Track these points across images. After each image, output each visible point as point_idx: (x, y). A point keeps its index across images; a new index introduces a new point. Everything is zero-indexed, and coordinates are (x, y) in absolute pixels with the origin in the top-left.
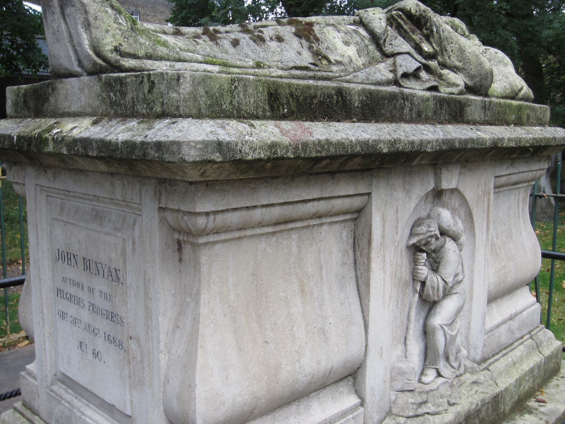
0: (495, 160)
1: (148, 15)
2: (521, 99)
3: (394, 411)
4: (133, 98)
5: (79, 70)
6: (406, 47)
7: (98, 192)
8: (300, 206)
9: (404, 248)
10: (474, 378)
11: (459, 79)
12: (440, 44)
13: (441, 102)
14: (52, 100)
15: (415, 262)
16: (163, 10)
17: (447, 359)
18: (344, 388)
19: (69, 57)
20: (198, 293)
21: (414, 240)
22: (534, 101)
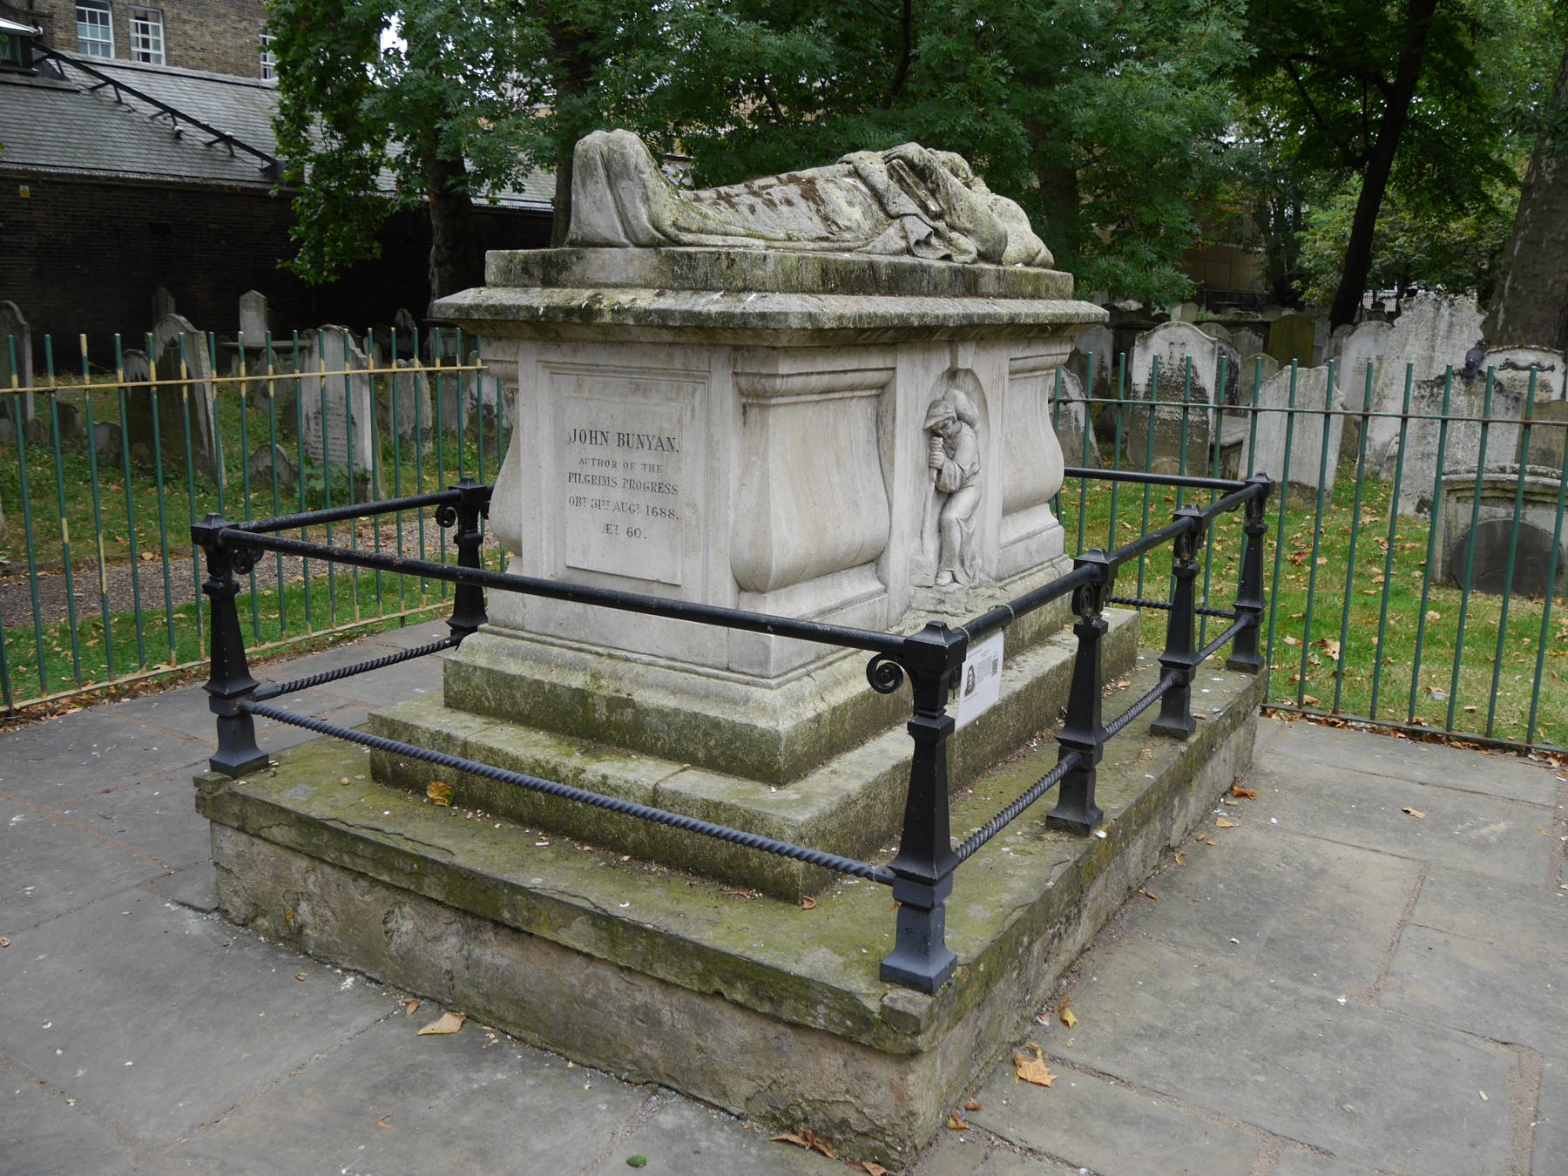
0: (499, 338)
1: (185, 22)
2: (1039, 265)
3: (914, 605)
5: (625, 241)
6: (912, 207)
7: (646, 363)
8: (842, 375)
9: (921, 432)
10: (991, 592)
11: (970, 244)
12: (947, 201)
13: (956, 272)
14: (577, 269)
15: (931, 447)
16: (223, 11)
17: (962, 563)
18: (868, 571)
19: (613, 228)
20: (766, 451)
21: (931, 423)
22: (1054, 268)
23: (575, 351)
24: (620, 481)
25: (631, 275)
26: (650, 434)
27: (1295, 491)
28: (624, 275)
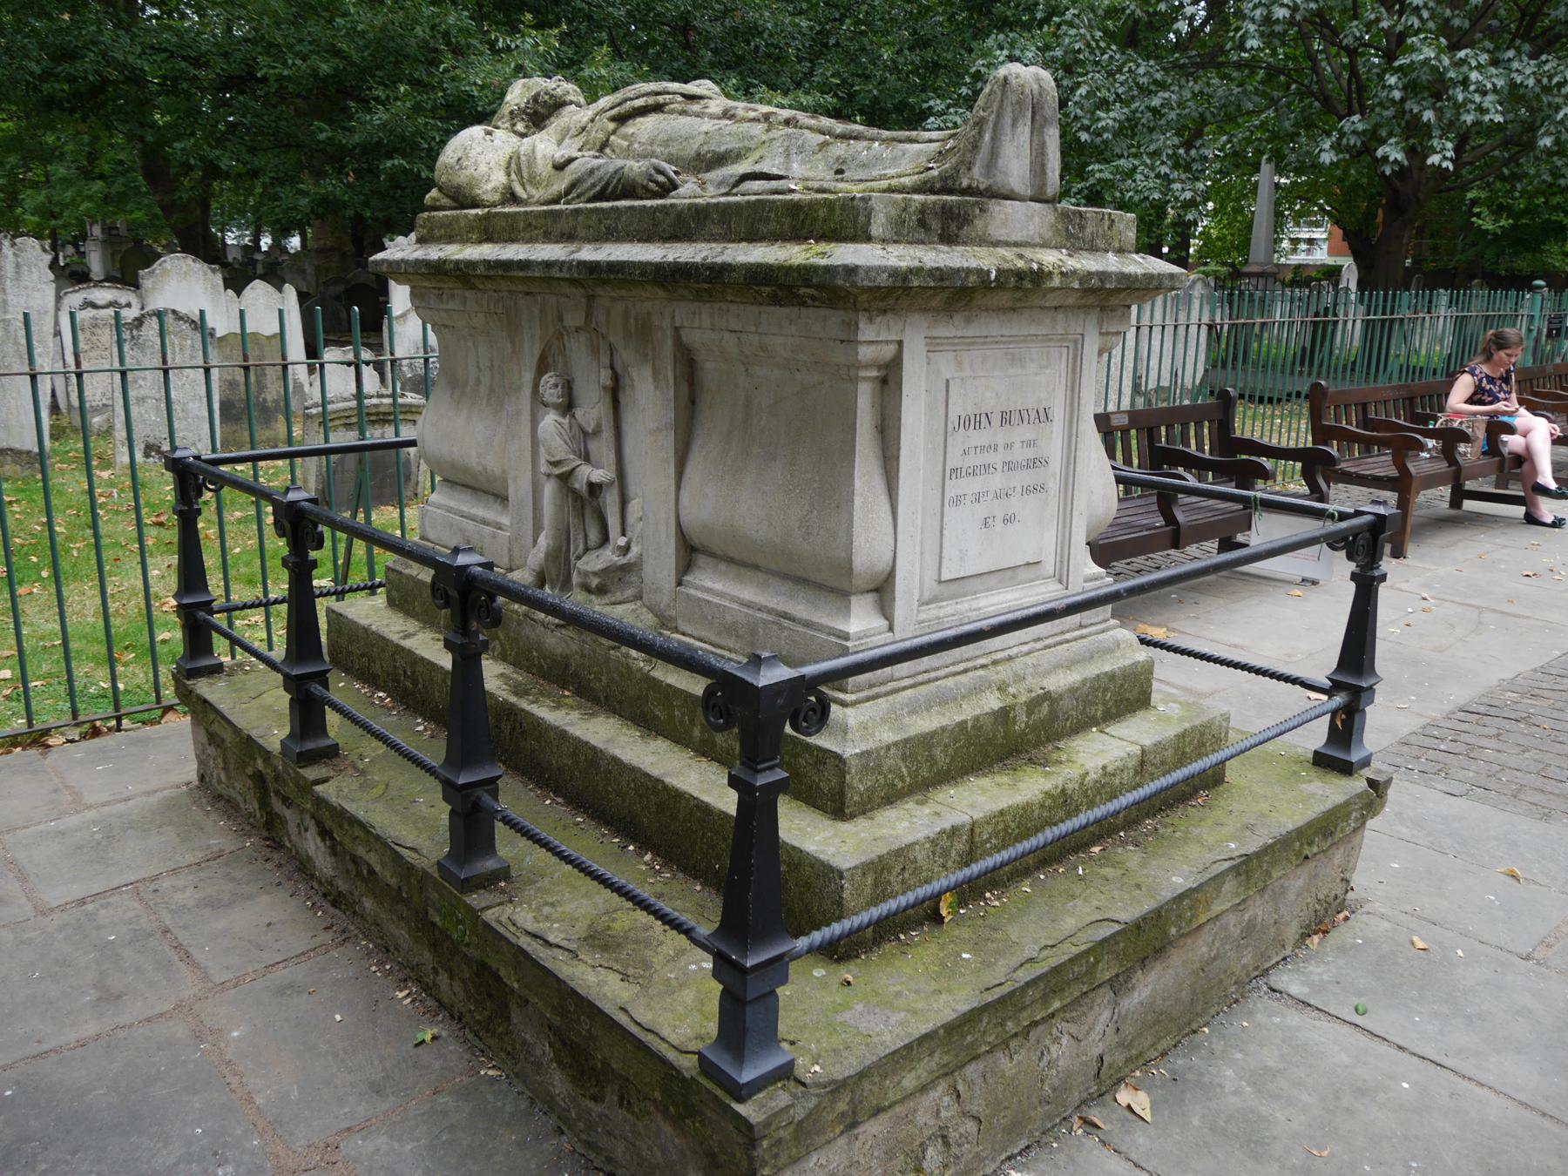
0: (884, 312)
4: (1092, 233)
14: (979, 223)
23: (968, 321)
24: (999, 467)
25: (1031, 233)
26: (1030, 407)
27: (9, 458)
28: (1025, 232)
